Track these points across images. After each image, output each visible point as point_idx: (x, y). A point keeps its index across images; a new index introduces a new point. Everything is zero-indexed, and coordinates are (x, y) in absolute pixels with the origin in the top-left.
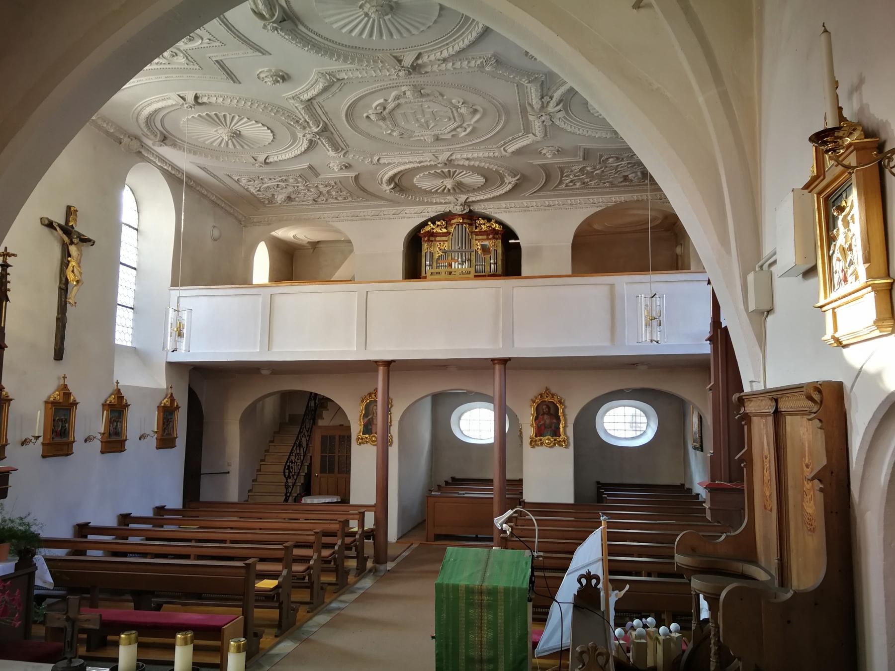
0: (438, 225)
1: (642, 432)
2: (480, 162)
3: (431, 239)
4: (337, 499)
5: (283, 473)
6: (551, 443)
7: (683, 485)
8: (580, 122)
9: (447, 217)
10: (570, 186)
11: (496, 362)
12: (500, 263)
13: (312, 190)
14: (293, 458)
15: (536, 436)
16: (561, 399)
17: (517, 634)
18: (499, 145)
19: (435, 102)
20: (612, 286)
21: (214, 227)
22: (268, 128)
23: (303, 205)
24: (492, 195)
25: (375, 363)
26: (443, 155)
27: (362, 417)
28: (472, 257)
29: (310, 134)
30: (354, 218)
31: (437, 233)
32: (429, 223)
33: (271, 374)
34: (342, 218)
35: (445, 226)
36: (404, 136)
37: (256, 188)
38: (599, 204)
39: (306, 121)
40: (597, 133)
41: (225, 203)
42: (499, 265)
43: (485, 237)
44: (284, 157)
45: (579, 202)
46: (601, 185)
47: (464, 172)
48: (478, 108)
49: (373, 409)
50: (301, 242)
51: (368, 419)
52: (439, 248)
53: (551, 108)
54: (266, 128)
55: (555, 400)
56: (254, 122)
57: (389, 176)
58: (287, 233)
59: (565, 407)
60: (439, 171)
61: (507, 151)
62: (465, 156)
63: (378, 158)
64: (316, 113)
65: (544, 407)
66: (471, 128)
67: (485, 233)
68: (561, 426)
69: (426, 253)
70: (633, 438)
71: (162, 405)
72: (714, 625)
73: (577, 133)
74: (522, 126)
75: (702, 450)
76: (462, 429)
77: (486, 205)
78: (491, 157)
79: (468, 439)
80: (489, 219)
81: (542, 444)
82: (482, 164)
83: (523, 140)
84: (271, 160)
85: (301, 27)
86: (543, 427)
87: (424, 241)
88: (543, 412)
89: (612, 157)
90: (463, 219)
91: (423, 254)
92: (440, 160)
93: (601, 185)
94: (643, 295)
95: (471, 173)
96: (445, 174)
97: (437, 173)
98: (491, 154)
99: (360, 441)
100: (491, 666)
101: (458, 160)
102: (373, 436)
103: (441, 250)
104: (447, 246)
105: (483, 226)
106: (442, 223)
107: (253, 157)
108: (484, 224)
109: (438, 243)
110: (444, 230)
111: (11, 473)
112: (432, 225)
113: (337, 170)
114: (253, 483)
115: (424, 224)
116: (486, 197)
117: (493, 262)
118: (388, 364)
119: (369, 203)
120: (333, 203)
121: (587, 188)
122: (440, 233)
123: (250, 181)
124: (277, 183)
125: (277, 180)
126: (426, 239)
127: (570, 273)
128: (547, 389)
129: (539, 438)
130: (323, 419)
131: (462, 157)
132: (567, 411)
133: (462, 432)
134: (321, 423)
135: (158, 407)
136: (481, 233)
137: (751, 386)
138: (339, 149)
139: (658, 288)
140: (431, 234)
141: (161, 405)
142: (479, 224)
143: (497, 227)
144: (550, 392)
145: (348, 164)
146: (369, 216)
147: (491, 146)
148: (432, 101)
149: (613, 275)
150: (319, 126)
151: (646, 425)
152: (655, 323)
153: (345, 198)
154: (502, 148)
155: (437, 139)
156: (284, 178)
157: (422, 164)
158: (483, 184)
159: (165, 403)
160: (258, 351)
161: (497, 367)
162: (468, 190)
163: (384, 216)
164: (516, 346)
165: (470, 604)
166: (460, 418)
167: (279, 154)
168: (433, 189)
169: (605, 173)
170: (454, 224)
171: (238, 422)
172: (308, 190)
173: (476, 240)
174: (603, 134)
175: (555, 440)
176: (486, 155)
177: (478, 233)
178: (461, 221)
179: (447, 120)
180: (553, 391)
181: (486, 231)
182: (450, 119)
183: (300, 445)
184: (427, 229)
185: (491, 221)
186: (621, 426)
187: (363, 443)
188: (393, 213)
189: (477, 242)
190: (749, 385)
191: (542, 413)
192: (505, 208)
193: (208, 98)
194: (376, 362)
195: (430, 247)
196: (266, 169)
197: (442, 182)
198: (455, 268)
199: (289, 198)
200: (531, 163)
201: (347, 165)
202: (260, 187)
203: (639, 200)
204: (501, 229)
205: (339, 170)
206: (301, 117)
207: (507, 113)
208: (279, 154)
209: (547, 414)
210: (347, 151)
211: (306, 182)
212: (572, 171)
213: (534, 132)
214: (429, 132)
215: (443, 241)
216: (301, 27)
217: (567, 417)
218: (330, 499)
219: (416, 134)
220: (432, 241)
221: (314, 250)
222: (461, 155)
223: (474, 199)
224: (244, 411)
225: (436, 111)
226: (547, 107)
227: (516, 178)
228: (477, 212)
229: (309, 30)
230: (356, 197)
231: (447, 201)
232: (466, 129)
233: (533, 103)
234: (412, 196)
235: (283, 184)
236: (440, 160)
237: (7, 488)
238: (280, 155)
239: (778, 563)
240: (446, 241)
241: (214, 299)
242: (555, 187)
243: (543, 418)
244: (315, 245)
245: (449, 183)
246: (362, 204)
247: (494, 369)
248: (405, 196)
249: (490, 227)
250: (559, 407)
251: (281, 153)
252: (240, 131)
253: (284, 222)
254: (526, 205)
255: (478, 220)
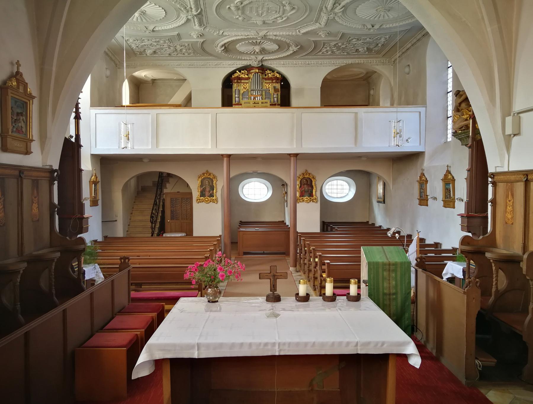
0: (243, 73)
1: (346, 194)
2: (282, 37)
3: (238, 81)
4: (185, 234)
5: (150, 221)
6: (308, 201)
7: (368, 222)
8: (350, 20)
9: (247, 68)
10: (325, 53)
11: (292, 155)
12: (280, 97)
13: (172, 48)
14: (154, 211)
15: (300, 197)
16: (314, 176)
17: (406, 281)
18: (297, 28)
19: (273, 2)
20: (356, 113)
21: (107, 68)
23: (161, 57)
24: (279, 56)
25: (221, 156)
26: (262, 32)
27: (199, 187)
28: (263, 93)
29: (191, 15)
30: (190, 66)
31: (242, 78)
32: (237, 71)
33: (149, 161)
34: (183, 66)
35: (247, 74)
36: (245, 20)
37: (136, 45)
38: (337, 64)
39: (191, 8)
40: (354, 25)
41: (112, 53)
42: (279, 99)
43: (271, 81)
44: (165, 28)
45: (325, 62)
46: (342, 54)
47: (269, 43)
48: (296, 7)
49: (205, 182)
50: (147, 79)
51: (203, 188)
52: (243, 87)
53: (336, 10)
54: (164, 10)
55: (211, 177)
56: (158, 6)
58: (142, 74)
59: (316, 180)
60: (251, 41)
61: (301, 32)
62: (275, 34)
63: (223, 31)
64: (199, 4)
65: (305, 180)
66: (286, 18)
67: (271, 79)
68: (314, 191)
69: (235, 90)
70: (341, 197)
71: (92, 180)
72: (496, 272)
73: (344, 25)
74: (315, 18)
75: (384, 203)
76: (244, 194)
77: (272, 62)
78: (290, 35)
79: (248, 199)
80: (273, 71)
81: (303, 201)
82: (282, 39)
83: (312, 26)
84: (157, 29)
86: (304, 192)
87: (234, 82)
88: (304, 183)
89: (355, 39)
90: (259, 70)
91: (234, 90)
92: (260, 35)
93: (342, 54)
94: (393, 121)
95: (273, 43)
96: (254, 43)
97: (250, 42)
98: (290, 33)
99: (198, 201)
100: (394, 296)
101: (269, 35)
102: (206, 198)
103: (244, 88)
104: (248, 86)
105: (269, 75)
106: (245, 72)
107: (145, 27)
108: (270, 73)
109: (243, 84)
110: (246, 76)
111: (89, 218)
112: (239, 73)
113: (195, 38)
114: (129, 227)
115: (234, 72)
116: (274, 57)
117: (276, 97)
118: (229, 156)
119: (202, 58)
120: (181, 56)
121: (334, 55)
122: (244, 78)
123: (135, 41)
124: (151, 43)
125: (152, 41)
126: (236, 81)
127: (319, 106)
128: (306, 171)
129: (301, 198)
130: (167, 188)
131: (280, 34)
132: (317, 183)
133: (244, 196)
134: (165, 191)
135: (90, 182)
136: (269, 79)
137: (496, 169)
138: (201, 25)
139: (400, 116)
140: (239, 78)
141: (91, 180)
142: (267, 73)
143: (278, 76)
144: (308, 172)
145: (202, 34)
146: (200, 65)
147: (292, 29)
148: (272, 1)
149: (357, 108)
150: (197, 11)
151: (348, 190)
152: (398, 136)
153: (189, 54)
154: (298, 30)
155: (264, 23)
156: (158, 40)
157: (248, 37)
158: (276, 50)
159: (93, 179)
160: (150, 148)
161: (292, 158)
162: (266, 53)
163: (210, 66)
164: (303, 146)
165: (384, 270)
166: (243, 188)
167: (163, 26)
168: (252, 52)
169: (347, 47)
170: (253, 72)
171: (121, 190)
172: (169, 48)
173: (265, 83)
174: (357, 26)
175: (310, 199)
176: (288, 33)
177: (267, 79)
178: (257, 71)
179: (274, 12)
180: (309, 172)
181: (271, 78)
182: (276, 12)
183: (156, 204)
184: (236, 75)
185: (274, 72)
186: (335, 191)
187: (200, 202)
188: (215, 64)
189: (266, 84)
190: (495, 168)
191: (303, 184)
192: (283, 64)
194: (222, 155)
195: (238, 86)
196: (153, 34)
197: (253, 48)
198: (260, 100)
199: (155, 52)
200: (309, 39)
201: (201, 34)
202: (139, 45)
203: (359, 63)
204: (280, 77)
205: (196, 38)
206: (189, 5)
207: (311, 11)
208: (163, 26)
209: (306, 185)
210: (206, 27)
211: (170, 43)
212: (329, 45)
213: (320, 23)
214: (260, 19)
215: (246, 83)
217: (317, 186)
218: (181, 234)
219: (253, 19)
220: (239, 83)
221: (153, 84)
222: (273, 33)
223: (267, 58)
224: (124, 184)
225: (270, 8)
226: (334, 9)
227: (298, 48)
228: (266, 65)
230: (196, 54)
231: (250, 58)
232: (283, 18)
233: (328, 7)
234: (231, 55)
235: (155, 44)
236: (260, 35)
237: (88, 227)
238: (163, 27)
239: (523, 245)
240: (248, 83)
241: (128, 116)
242: (316, 53)
243: (304, 186)
244: (154, 81)
245: (257, 49)
246: (198, 58)
247: (290, 160)
248: (228, 55)
249: (273, 75)
250: (313, 180)
251: (165, 25)
252: (145, 11)
253: (143, 67)
254: (295, 63)
255: (267, 71)
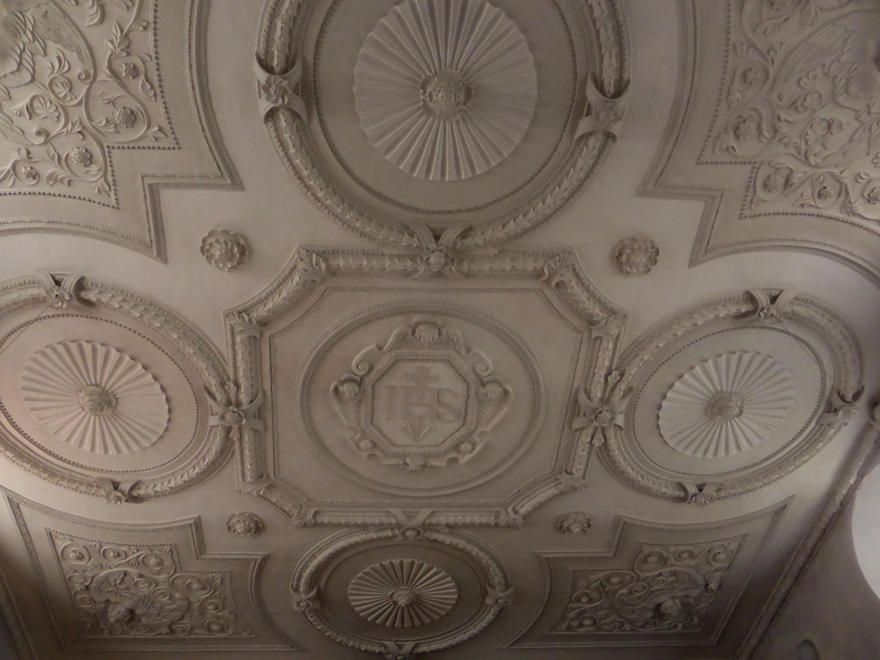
22: (168, 400)
57: (308, 575)
85: (316, 124)
193: (100, 292)
216: (316, 124)
229: (326, 135)
